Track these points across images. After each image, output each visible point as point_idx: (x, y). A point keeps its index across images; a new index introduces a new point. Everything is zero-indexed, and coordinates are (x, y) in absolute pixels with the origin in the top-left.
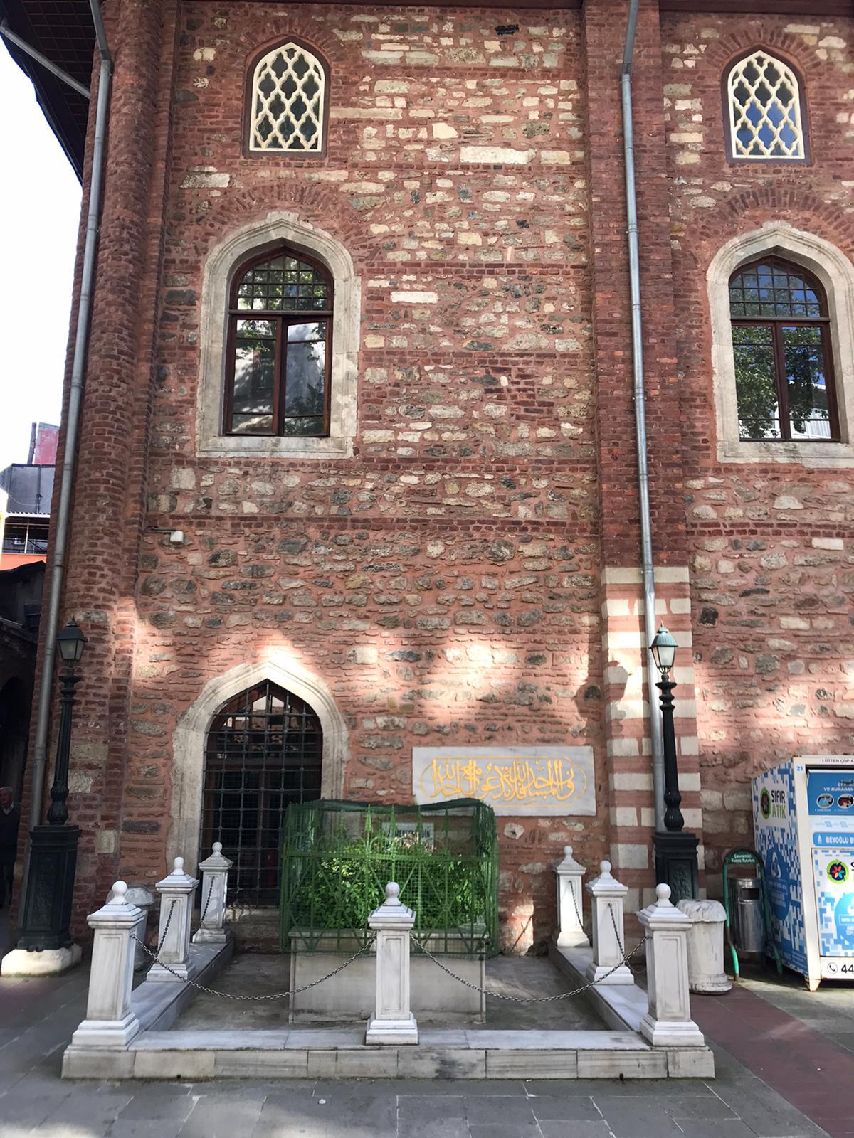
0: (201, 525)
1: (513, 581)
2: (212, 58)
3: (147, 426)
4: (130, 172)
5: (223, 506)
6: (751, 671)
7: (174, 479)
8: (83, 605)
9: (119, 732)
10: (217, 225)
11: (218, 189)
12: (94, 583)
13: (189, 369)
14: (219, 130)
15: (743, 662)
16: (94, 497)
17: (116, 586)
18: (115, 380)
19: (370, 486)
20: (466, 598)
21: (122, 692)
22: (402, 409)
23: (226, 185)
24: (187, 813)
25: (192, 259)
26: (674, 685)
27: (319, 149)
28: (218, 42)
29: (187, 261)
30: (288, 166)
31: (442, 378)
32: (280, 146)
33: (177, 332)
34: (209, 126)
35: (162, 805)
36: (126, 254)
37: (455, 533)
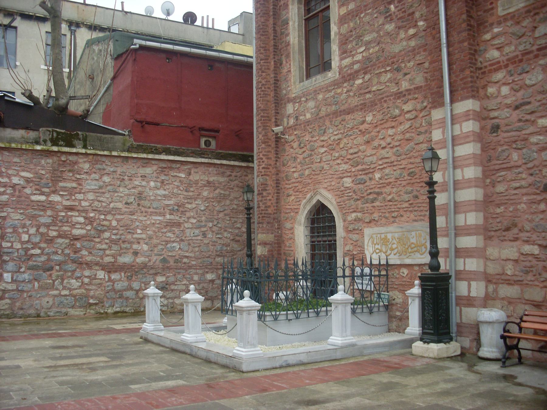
1: (401, 128)
6: (519, 163)
15: (515, 156)
17: (270, 165)
19: (345, 90)
20: (383, 144)
22: (354, 43)
26: (436, 182)
31: (367, 18)
37: (376, 106)
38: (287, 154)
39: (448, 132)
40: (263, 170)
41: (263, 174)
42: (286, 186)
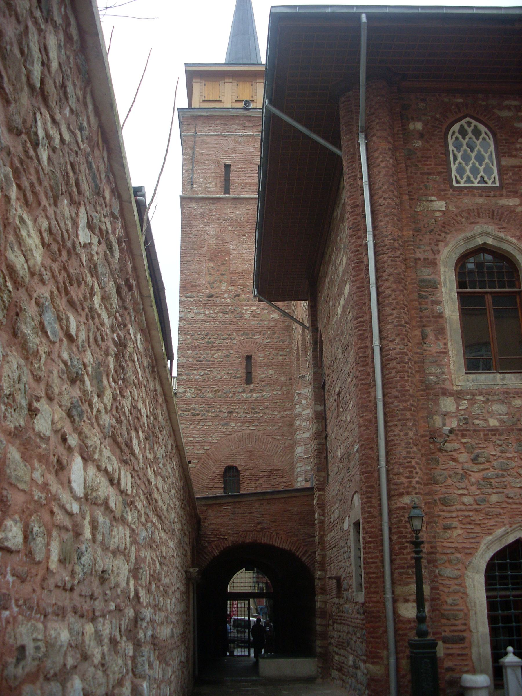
0: (463, 436)
2: (421, 128)
3: (422, 371)
4: (393, 204)
5: (477, 422)
7: (442, 406)
8: (408, 493)
9: (436, 576)
10: (443, 235)
11: (439, 211)
12: (413, 477)
13: (441, 331)
14: (433, 173)
16: (403, 421)
18: (406, 341)
21: (434, 550)
23: (444, 209)
24: (481, 629)
25: (431, 257)
27: (497, 185)
28: (424, 118)
29: (428, 259)
30: (481, 196)
32: (473, 183)
33: (429, 306)
34: (426, 171)
35: (465, 624)
36: (398, 257)
38: (441, 467)
39: (359, 228)
40: (417, 486)
41: (417, 491)
42: (441, 513)
